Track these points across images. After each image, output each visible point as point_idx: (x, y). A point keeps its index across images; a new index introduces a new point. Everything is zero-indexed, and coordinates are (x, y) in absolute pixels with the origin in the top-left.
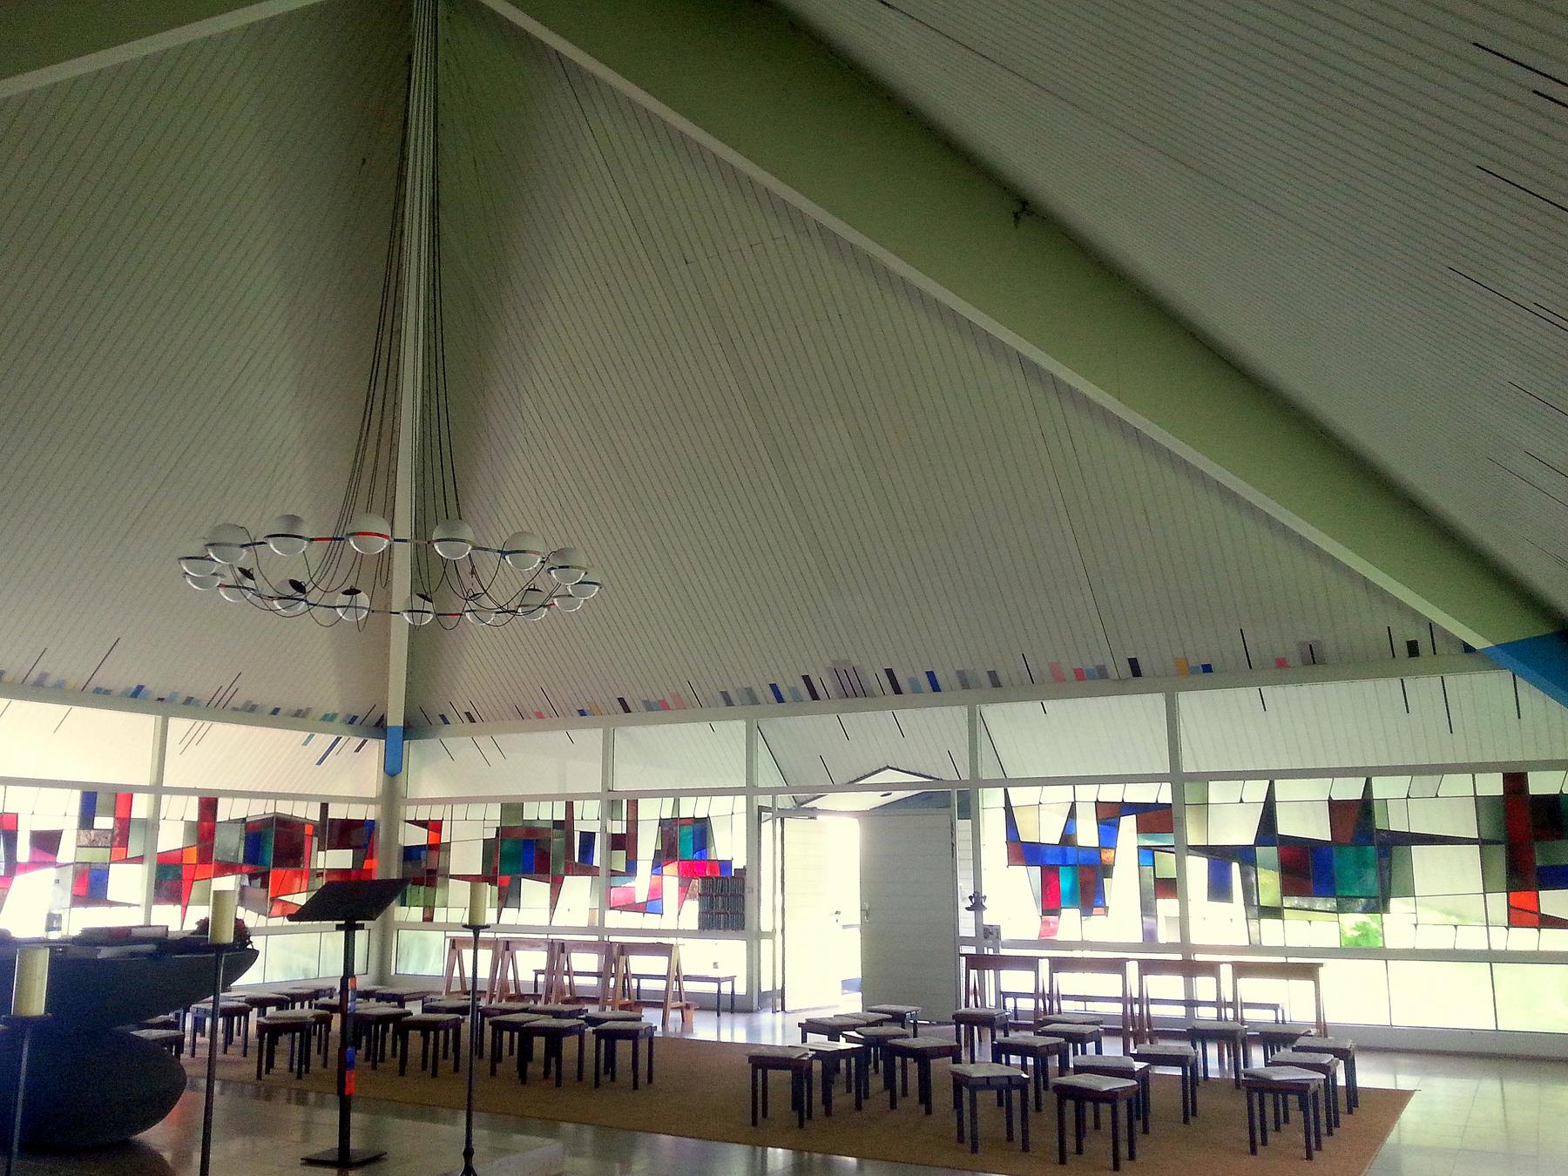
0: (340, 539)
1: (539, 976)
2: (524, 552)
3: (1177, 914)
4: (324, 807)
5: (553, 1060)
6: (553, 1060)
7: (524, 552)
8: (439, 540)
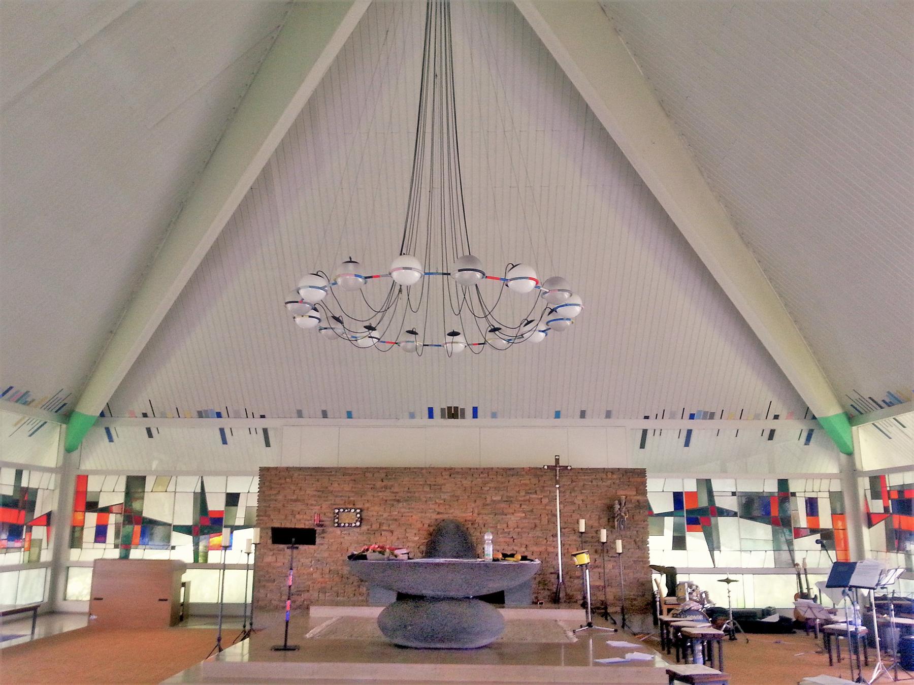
4: (19, 474)
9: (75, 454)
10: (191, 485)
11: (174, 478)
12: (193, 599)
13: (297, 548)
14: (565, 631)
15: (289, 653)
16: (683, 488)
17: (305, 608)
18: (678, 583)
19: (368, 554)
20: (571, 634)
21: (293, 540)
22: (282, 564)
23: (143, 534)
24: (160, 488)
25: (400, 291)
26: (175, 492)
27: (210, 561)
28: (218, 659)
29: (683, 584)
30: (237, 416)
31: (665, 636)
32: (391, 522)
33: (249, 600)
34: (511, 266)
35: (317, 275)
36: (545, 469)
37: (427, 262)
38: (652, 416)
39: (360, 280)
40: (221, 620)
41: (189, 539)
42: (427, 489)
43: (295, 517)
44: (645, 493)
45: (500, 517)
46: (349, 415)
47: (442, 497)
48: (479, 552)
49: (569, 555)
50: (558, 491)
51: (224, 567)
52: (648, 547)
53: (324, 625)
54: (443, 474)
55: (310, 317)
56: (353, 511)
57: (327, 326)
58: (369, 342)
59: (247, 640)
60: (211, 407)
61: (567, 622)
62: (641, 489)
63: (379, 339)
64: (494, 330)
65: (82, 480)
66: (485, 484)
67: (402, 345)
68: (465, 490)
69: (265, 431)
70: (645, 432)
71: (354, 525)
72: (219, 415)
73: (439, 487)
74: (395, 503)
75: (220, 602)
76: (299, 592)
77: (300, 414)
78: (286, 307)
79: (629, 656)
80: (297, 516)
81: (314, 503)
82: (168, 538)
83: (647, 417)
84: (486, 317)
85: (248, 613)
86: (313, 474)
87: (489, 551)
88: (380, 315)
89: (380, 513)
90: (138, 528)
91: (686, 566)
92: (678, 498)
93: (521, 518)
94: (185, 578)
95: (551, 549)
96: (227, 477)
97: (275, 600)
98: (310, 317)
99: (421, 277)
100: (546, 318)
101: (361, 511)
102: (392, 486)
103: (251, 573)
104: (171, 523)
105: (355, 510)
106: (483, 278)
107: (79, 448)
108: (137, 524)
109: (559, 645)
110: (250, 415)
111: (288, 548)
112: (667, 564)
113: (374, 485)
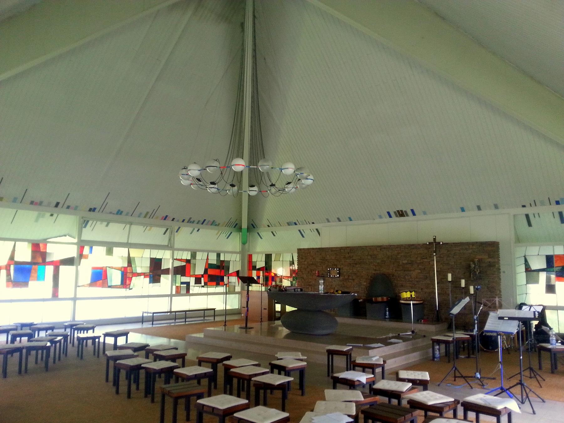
0: (227, 167)
1: (344, 358)
2: (288, 168)
3: (172, 311)
4: (218, 255)
5: (228, 386)
6: (213, 384)
7: (288, 168)
8: (260, 166)
9: (247, 245)
11: (282, 254)
16: (554, 252)
32: (353, 275)
38: (528, 205)
42: (369, 257)
43: (312, 272)
45: (407, 272)
47: (377, 262)
50: (435, 257)
54: (377, 249)
65: (250, 256)
66: (398, 254)
68: (388, 258)
71: (336, 276)
72: (296, 224)
73: (375, 256)
74: (354, 265)
75: (225, 309)
80: (313, 272)
83: (524, 206)
86: (319, 251)
91: (147, 295)
92: (550, 260)
96: (553, 247)
101: (339, 269)
107: (248, 242)
113: (345, 256)
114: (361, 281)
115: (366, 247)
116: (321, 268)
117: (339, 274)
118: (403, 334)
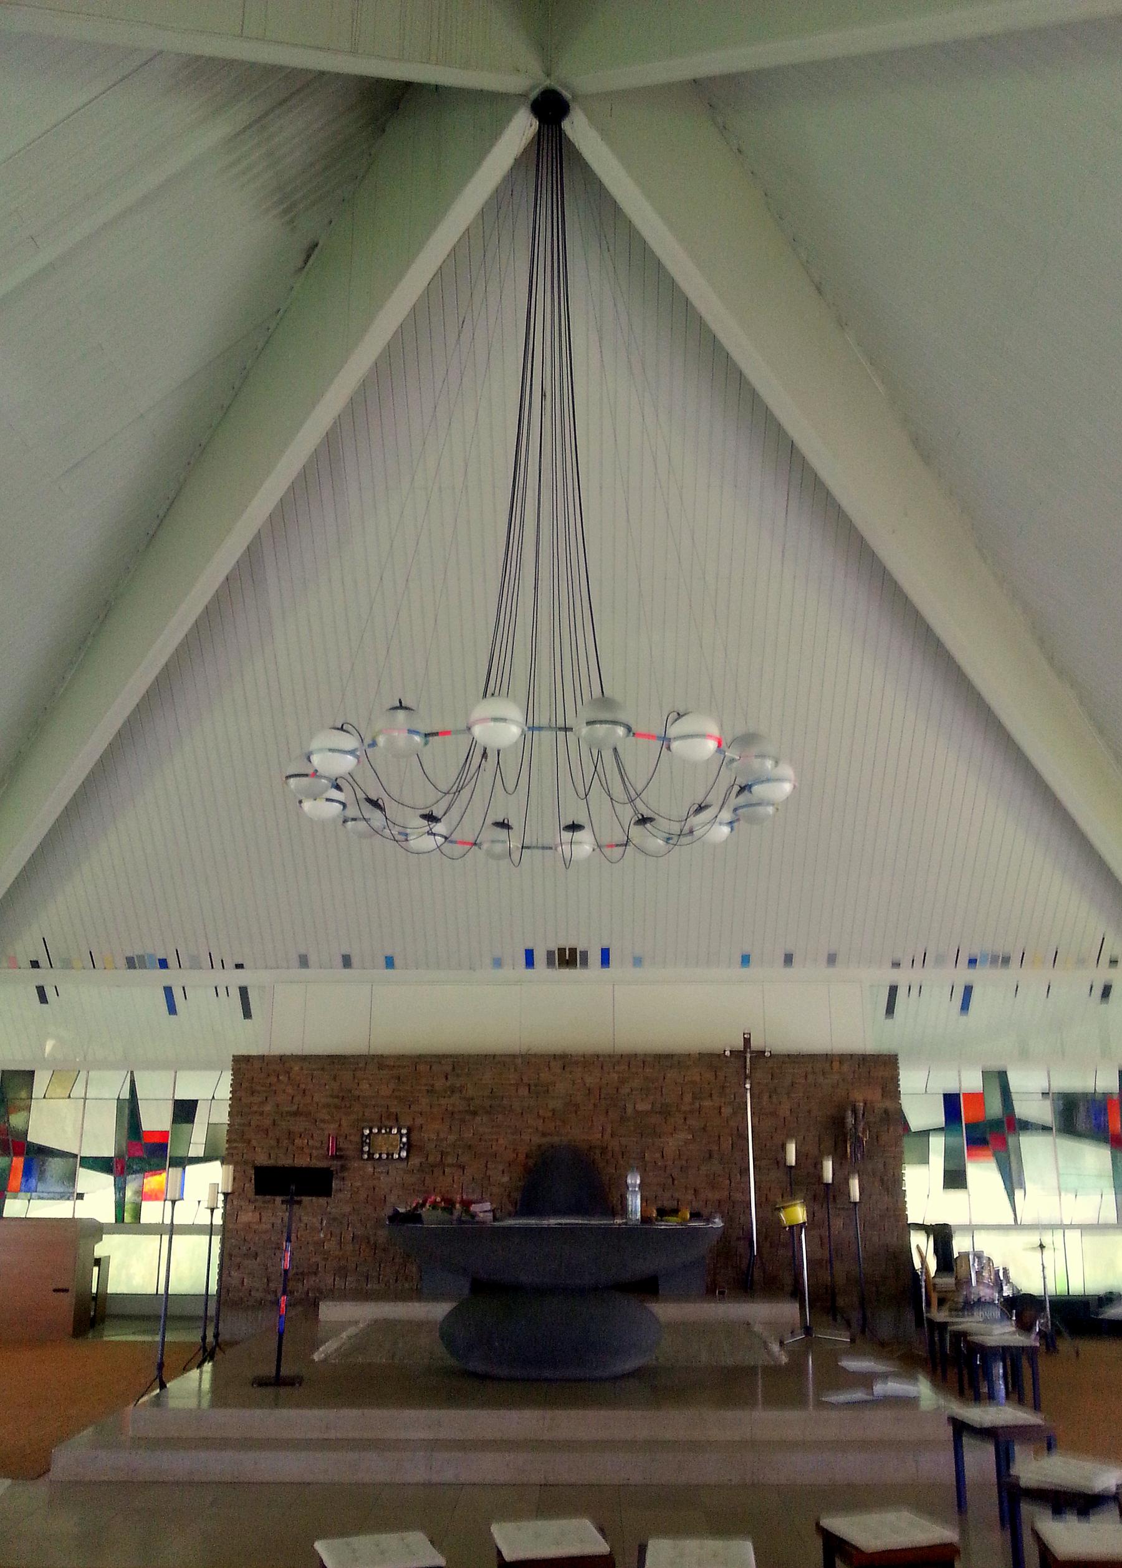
10: (114, 1087)
11: (83, 1074)
12: (115, 1286)
13: (299, 1203)
14: (765, 1342)
15: (283, 1391)
17: (312, 1305)
18: (956, 1255)
19: (425, 1212)
20: (775, 1348)
21: (293, 1187)
22: (269, 1226)
23: (28, 1172)
24: (59, 1092)
25: (485, 755)
26: (85, 1099)
27: (144, 1219)
28: (158, 1402)
29: (964, 1256)
30: (196, 965)
31: (937, 1347)
33: (213, 1288)
34: (674, 715)
35: (342, 729)
36: (726, 1057)
37: (528, 710)
39: (417, 738)
40: (164, 1325)
41: (108, 1180)
42: (523, 1091)
44: (896, 1094)
46: (390, 963)
48: (615, 1201)
49: (770, 1207)
51: (172, 1230)
52: (905, 1191)
53: (344, 1335)
55: (328, 800)
56: (395, 1131)
57: (358, 814)
58: (429, 843)
59: (208, 1367)
60: (150, 951)
61: (769, 1324)
62: (891, 1088)
63: (446, 838)
64: (643, 821)
66: (623, 1081)
67: (485, 846)
69: (244, 991)
70: (893, 990)
71: (396, 1156)
72: (163, 964)
75: (162, 1291)
76: (301, 1276)
77: (304, 962)
78: (287, 784)
79: (879, 1388)
80: (298, 1141)
81: (327, 1117)
82: (72, 1178)
84: (632, 801)
85: (212, 1311)
87: (635, 1203)
88: (449, 797)
89: (442, 1135)
90: (19, 1162)
92: (951, 1103)
93: (686, 1142)
94: (99, 1251)
95: (737, 1196)
97: (258, 1290)
98: (328, 800)
99: (522, 735)
100: (733, 801)
102: (462, 1087)
103: (216, 1240)
104: (76, 1152)
105: (399, 1131)
106: (628, 736)
108: (17, 1154)
109: (753, 1370)
110: (217, 963)
111: (283, 1202)
112: (932, 1219)
114: (489, 1173)
115: (514, 1056)
116: (333, 1126)
117: (409, 1147)
118: (825, 1337)
